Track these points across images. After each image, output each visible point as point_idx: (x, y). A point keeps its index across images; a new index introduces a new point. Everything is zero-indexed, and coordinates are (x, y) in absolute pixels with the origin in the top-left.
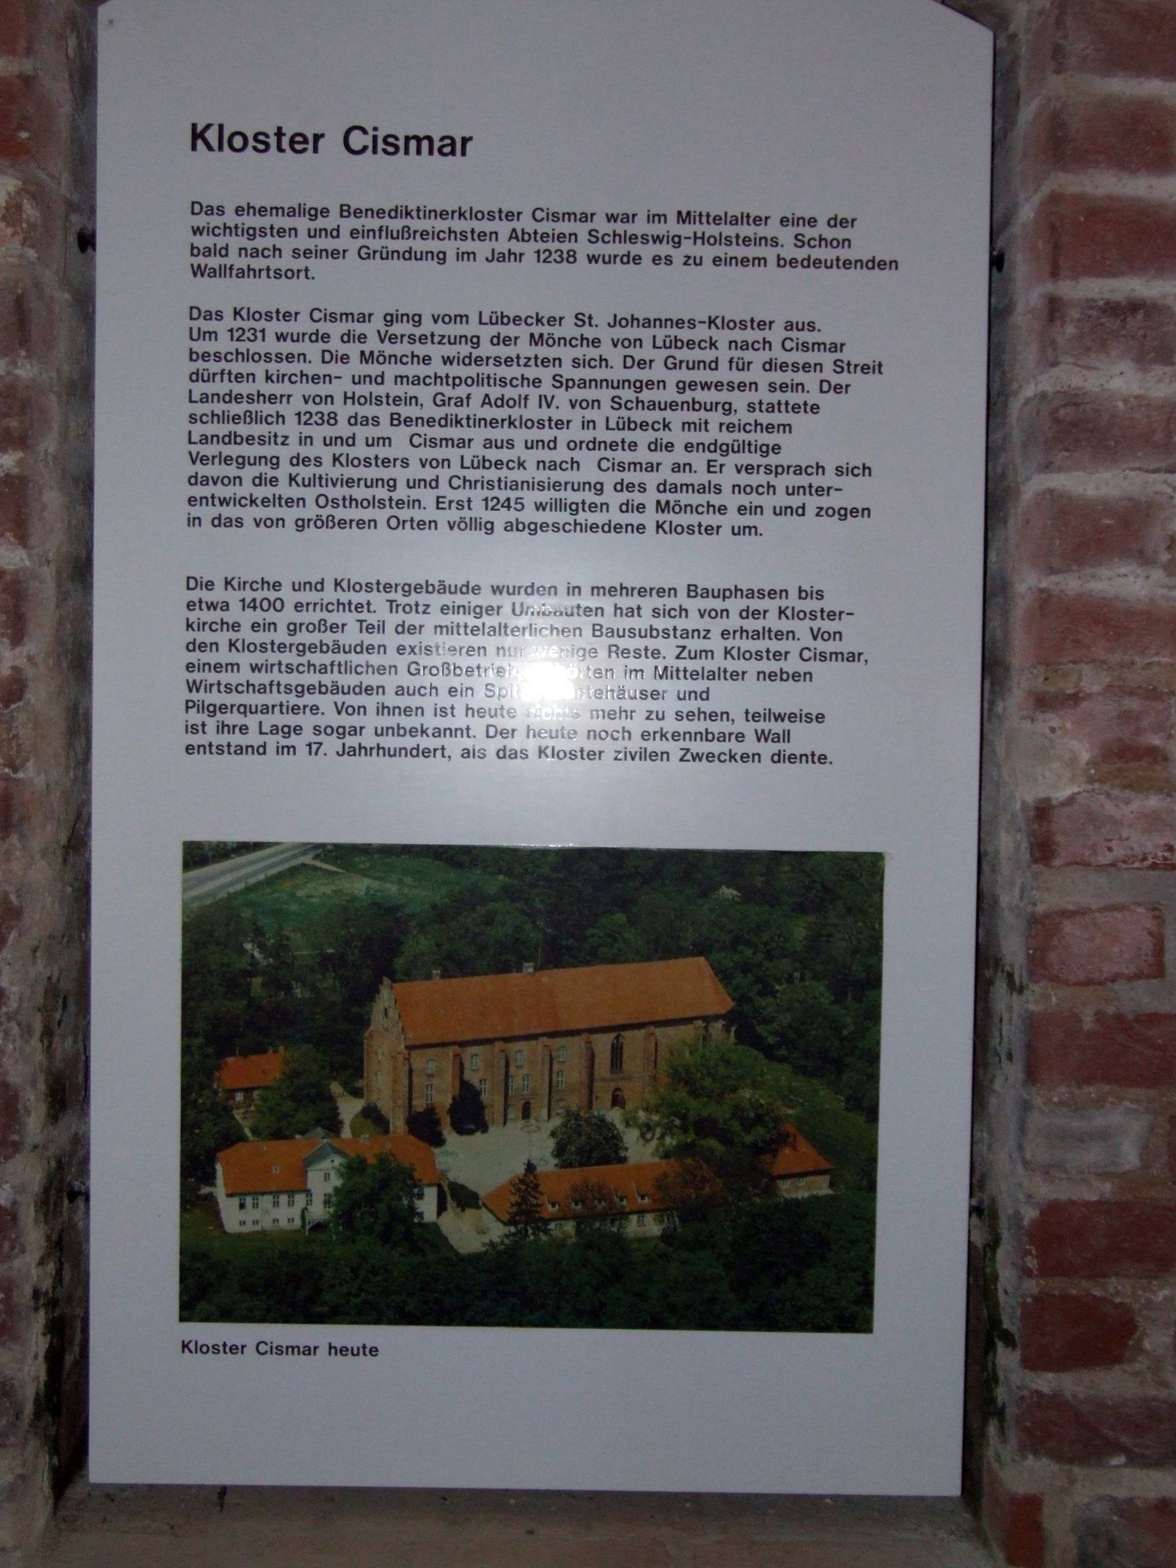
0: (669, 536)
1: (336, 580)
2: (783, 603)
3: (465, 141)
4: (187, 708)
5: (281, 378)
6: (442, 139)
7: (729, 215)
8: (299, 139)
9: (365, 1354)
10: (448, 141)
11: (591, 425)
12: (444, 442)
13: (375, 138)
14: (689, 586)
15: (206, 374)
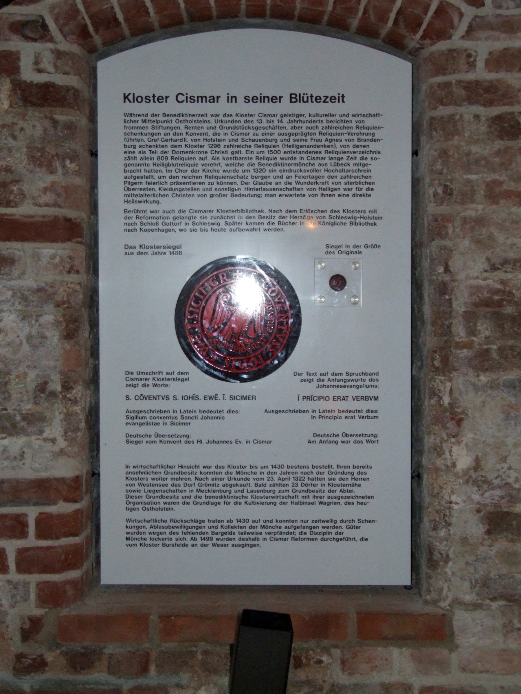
0: (132, 104)
1: (124, 94)
2: (222, 524)
3: (218, 97)
6: (210, 97)
9: (312, 102)
10: (212, 98)
11: (234, 99)
12: (200, 99)
13: (187, 97)
14: (291, 95)
15: (305, 97)
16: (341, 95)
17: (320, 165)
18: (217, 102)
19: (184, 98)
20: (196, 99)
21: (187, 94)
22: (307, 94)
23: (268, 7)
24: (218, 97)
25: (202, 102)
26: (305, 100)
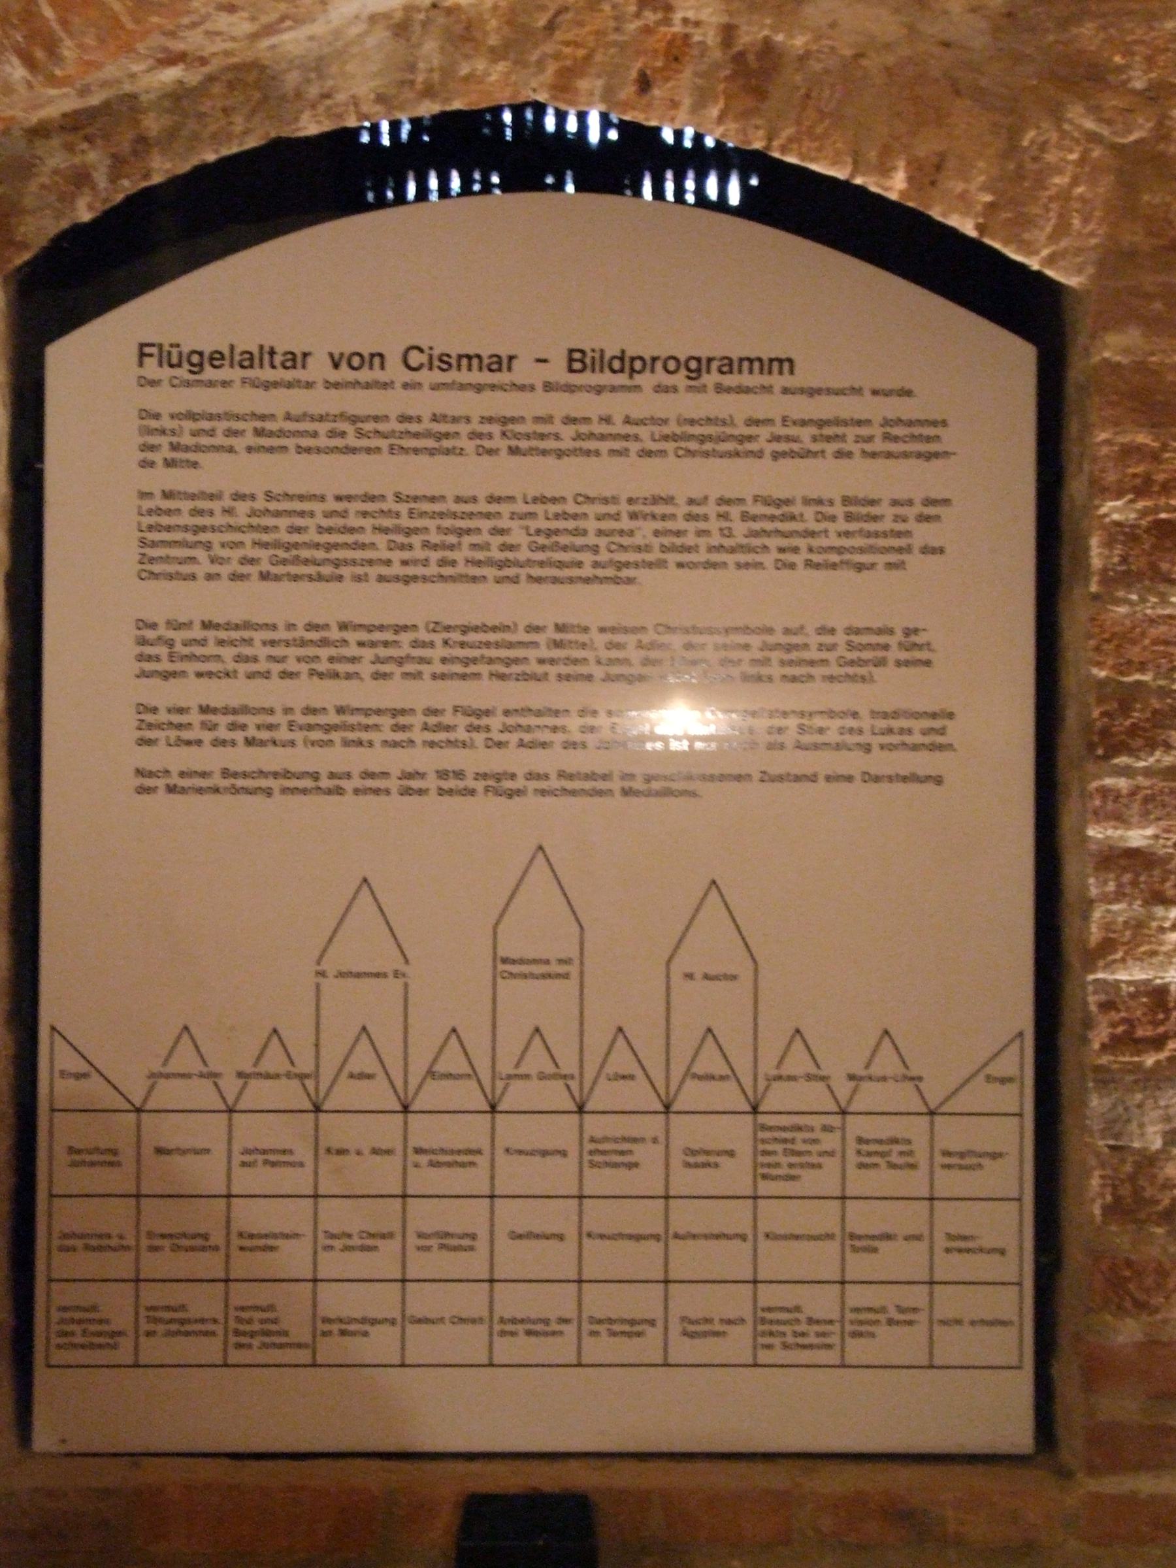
3: (511, 358)
4: (142, 355)
5: (423, 514)
7: (238, 351)
8: (218, 356)
11: (377, 360)
12: (464, 362)
13: (431, 357)
15: (175, 351)
16: (267, 349)
17: (388, 563)
18: (304, 367)
19: (424, 358)
20: (454, 362)
21: (431, 348)
22: (178, 346)
23: (318, 28)
24: (511, 358)
25: (470, 369)
26: (175, 360)
